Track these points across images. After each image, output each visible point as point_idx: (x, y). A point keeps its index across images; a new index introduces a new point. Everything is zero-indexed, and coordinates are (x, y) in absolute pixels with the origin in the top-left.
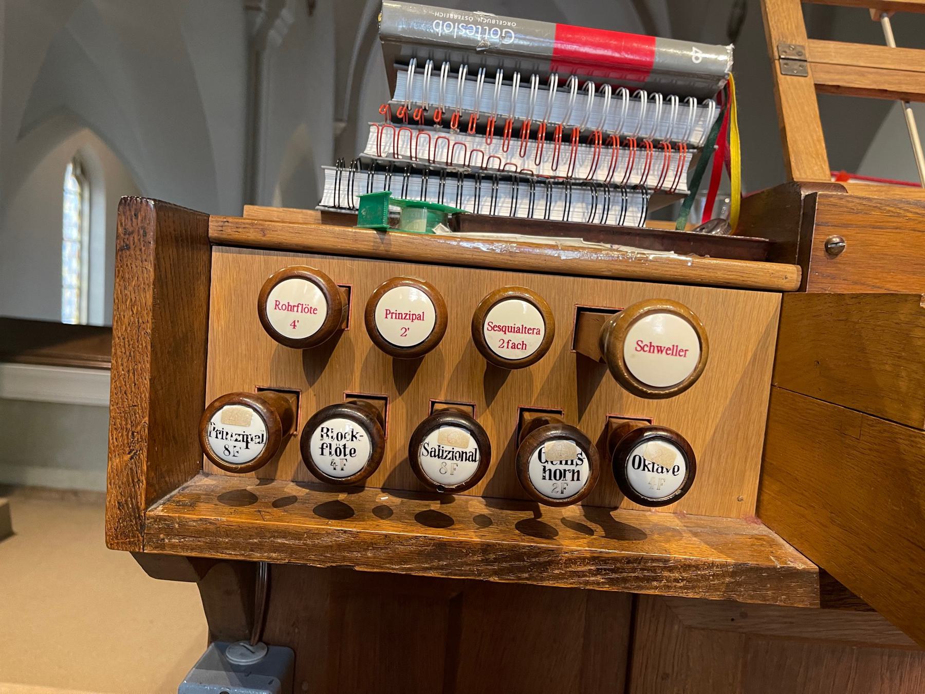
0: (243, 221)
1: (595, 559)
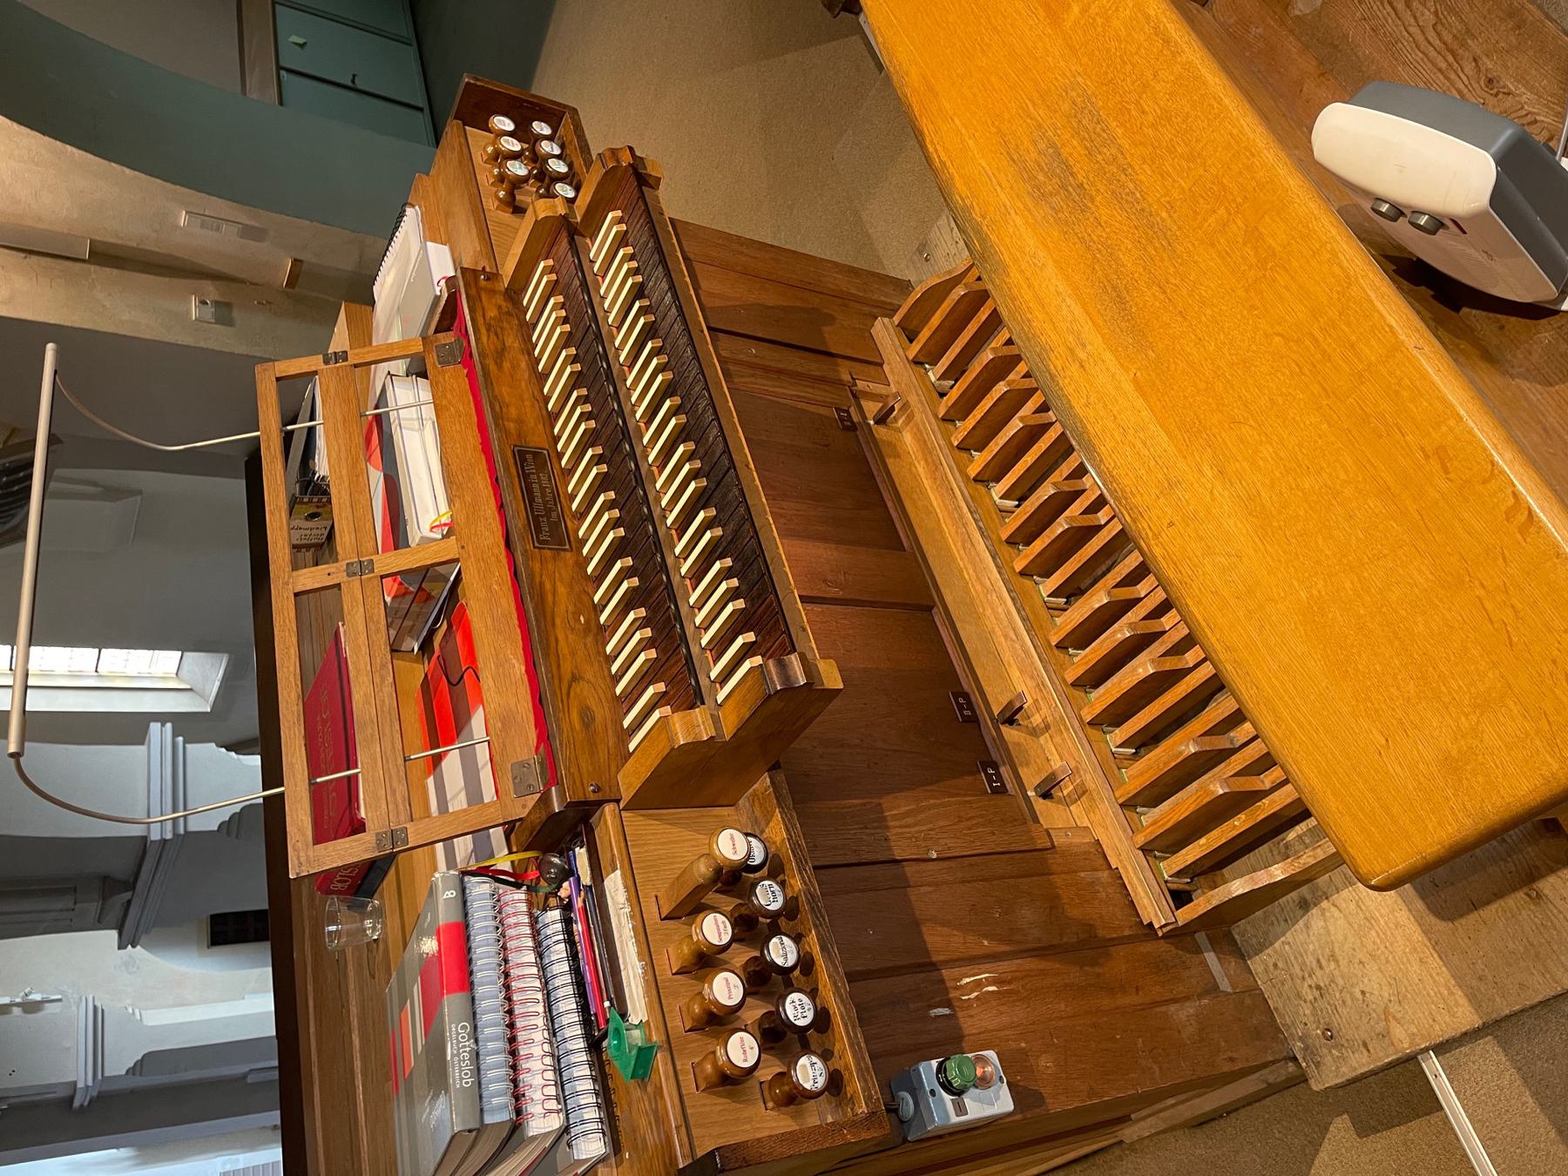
0: (1105, 491)
1: (801, 873)
